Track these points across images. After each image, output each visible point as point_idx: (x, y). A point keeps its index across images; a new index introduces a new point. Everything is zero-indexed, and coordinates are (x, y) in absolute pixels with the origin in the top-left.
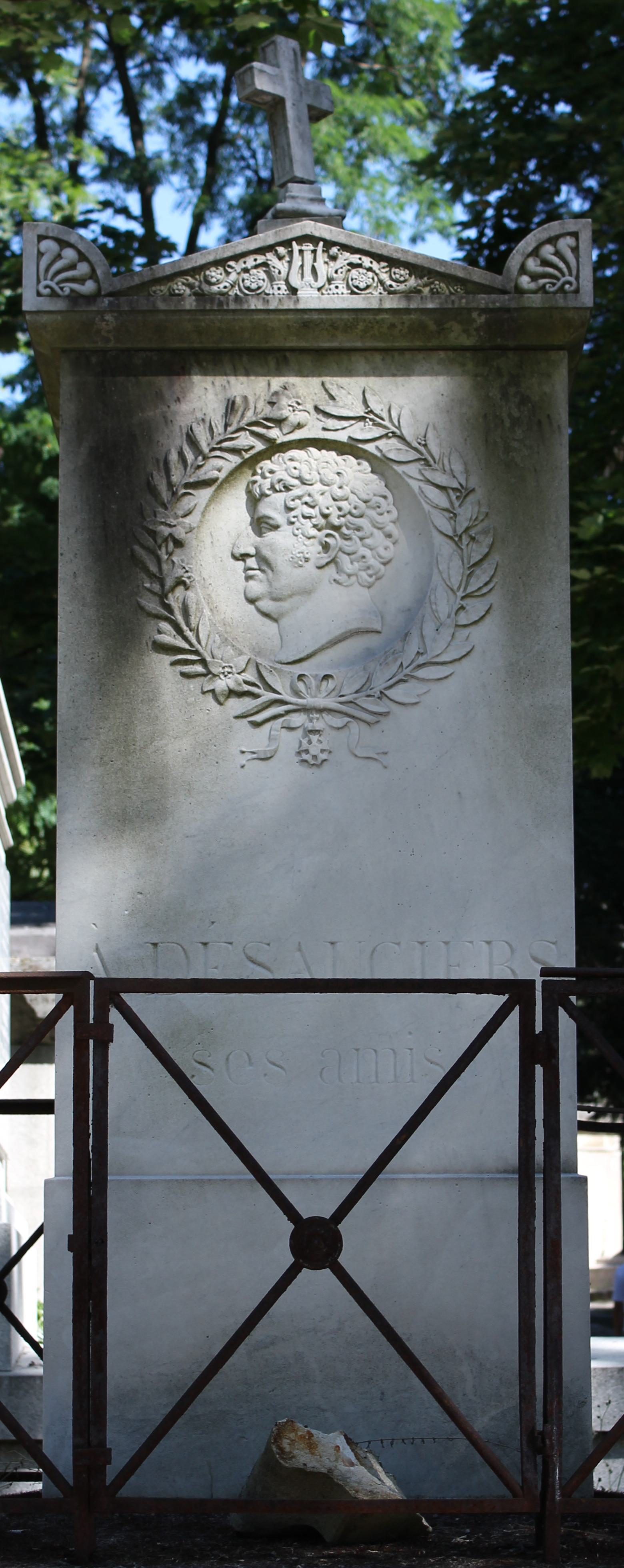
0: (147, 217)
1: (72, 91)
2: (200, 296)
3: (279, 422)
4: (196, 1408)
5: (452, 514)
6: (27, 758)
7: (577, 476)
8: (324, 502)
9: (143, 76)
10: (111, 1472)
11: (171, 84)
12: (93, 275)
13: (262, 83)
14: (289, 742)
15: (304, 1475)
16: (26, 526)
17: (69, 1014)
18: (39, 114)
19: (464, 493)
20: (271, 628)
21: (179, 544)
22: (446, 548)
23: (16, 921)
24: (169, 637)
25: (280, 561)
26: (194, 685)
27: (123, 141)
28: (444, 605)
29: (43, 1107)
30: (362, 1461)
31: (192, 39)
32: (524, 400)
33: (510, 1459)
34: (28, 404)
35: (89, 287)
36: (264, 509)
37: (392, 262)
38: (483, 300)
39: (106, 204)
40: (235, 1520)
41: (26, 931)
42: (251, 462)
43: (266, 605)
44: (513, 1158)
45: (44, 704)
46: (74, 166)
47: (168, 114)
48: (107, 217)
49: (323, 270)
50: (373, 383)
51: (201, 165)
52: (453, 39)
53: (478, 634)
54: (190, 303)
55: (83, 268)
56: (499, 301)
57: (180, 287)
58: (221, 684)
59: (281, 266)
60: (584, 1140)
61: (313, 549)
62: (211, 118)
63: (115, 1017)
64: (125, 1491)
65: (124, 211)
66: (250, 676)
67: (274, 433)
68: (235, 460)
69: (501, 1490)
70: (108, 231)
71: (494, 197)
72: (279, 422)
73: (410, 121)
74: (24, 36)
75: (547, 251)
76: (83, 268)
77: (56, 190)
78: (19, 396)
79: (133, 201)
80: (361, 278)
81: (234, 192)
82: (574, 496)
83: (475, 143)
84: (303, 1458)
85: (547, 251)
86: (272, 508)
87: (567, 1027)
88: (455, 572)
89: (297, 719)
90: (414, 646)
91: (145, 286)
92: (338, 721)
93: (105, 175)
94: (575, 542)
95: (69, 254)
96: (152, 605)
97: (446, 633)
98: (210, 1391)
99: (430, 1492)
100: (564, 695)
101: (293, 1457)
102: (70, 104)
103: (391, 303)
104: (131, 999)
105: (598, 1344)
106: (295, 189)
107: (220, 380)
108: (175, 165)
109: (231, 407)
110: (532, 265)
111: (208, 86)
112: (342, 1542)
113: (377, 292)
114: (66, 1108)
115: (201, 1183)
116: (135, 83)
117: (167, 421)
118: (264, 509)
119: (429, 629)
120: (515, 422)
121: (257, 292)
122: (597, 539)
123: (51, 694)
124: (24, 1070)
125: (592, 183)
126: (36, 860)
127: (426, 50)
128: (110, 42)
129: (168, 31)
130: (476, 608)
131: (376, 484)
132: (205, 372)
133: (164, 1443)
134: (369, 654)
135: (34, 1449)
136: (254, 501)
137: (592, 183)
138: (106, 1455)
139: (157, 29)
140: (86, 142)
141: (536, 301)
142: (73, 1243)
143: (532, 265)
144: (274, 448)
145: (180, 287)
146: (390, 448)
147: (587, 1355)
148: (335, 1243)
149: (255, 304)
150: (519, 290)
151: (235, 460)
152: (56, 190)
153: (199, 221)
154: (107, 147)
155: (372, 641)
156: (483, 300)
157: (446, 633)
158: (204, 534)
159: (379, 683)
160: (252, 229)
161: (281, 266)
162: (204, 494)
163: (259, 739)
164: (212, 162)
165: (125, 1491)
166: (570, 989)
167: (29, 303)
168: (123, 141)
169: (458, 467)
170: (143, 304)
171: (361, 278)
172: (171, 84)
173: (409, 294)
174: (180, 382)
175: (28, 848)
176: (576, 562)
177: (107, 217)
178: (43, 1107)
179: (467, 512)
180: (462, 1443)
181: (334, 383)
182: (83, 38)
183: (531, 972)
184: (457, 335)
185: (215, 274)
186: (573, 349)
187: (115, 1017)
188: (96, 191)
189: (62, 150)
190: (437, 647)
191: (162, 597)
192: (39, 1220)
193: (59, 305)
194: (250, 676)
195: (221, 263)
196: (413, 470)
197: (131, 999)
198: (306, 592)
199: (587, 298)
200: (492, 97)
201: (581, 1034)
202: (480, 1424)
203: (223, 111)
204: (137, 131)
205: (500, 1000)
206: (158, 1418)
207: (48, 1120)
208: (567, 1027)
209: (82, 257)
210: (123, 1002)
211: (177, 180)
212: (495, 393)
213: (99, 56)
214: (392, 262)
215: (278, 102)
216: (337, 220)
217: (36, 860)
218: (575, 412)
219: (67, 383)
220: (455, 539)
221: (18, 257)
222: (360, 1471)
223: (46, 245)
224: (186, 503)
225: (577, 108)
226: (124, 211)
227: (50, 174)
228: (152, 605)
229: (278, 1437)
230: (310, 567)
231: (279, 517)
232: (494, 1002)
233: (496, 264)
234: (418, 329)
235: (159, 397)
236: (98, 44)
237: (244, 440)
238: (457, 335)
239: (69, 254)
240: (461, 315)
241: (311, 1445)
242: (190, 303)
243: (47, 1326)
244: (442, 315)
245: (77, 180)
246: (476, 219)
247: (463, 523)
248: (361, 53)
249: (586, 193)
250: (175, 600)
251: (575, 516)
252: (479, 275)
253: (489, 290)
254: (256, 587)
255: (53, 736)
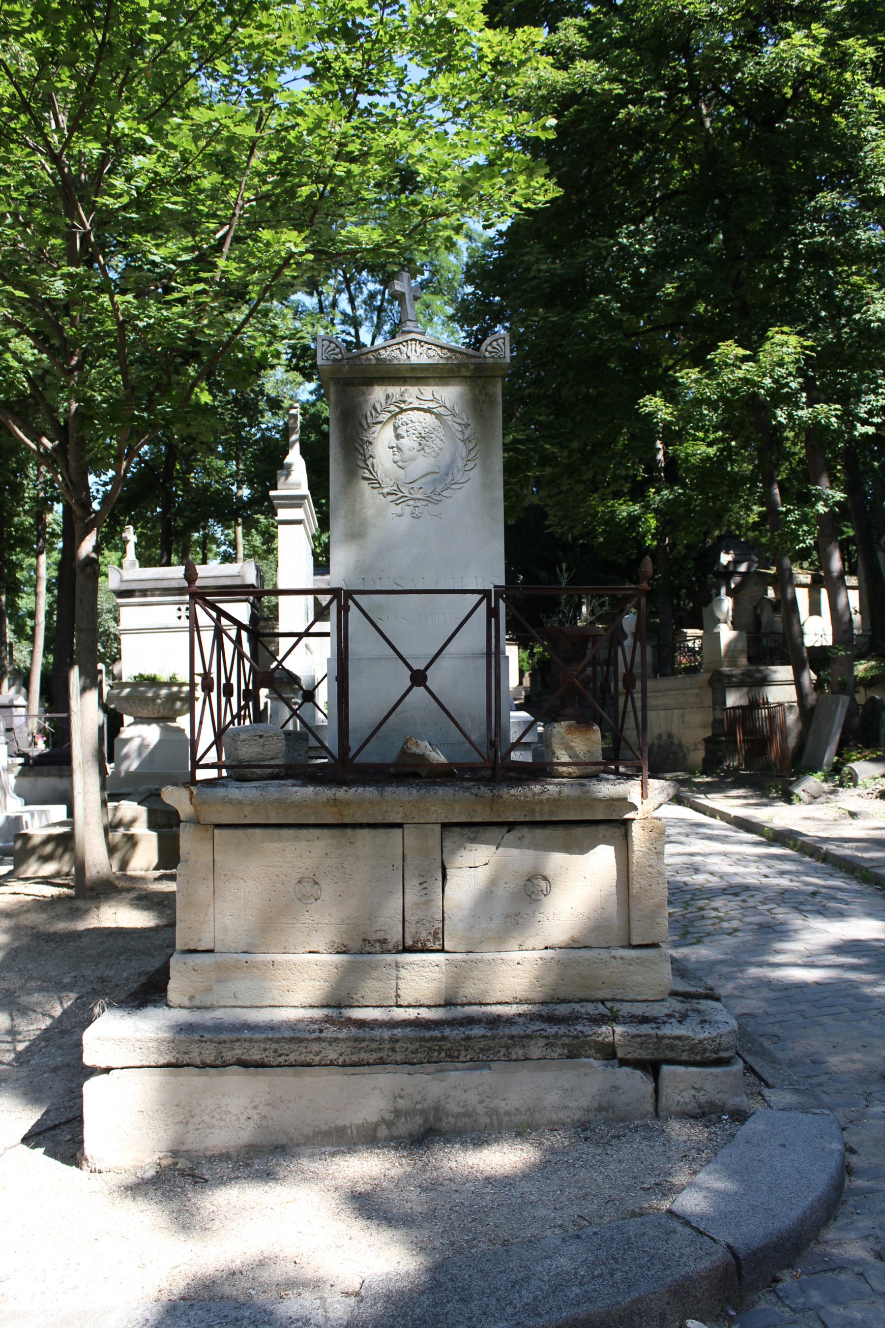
0: (357, 336)
1: (332, 294)
2: (377, 359)
3: (404, 402)
4: (379, 734)
5: (463, 433)
6: (318, 519)
7: (505, 422)
8: (420, 429)
9: (355, 289)
10: (351, 754)
11: (365, 291)
12: (341, 352)
13: (397, 288)
14: (408, 510)
15: (415, 755)
16: (317, 441)
17: (335, 602)
18: (320, 302)
19: (467, 426)
20: (402, 471)
21: (370, 443)
22: (461, 444)
23: (315, 574)
24: (367, 475)
25: (405, 449)
26: (376, 491)
27: (349, 311)
28: (460, 463)
29: (326, 635)
30: (434, 750)
31: (373, 276)
32: (487, 394)
33: (484, 749)
34: (317, 400)
35: (339, 356)
36: (399, 431)
37: (442, 348)
38: (473, 360)
39: (343, 332)
40: (392, 770)
41: (318, 577)
42: (395, 416)
43: (400, 464)
44: (484, 650)
45: (323, 501)
46: (332, 320)
47: (365, 302)
48: (344, 336)
49: (419, 350)
50: (436, 388)
51: (375, 319)
52: (461, 277)
53: (471, 473)
54: (374, 362)
55: (337, 350)
56: (479, 361)
57: (370, 356)
58: (385, 491)
59: (404, 349)
60: (508, 648)
61: (416, 445)
62: (379, 303)
63: (350, 603)
64: (355, 761)
65: (349, 334)
66: (395, 488)
67: (402, 406)
68: (389, 415)
69: (482, 760)
70: (344, 341)
71: (475, 328)
72: (404, 402)
73: (446, 303)
74: (316, 273)
75: (495, 344)
76: (337, 350)
77: (326, 328)
78: (314, 397)
79: (353, 332)
80: (431, 353)
81: (387, 328)
82: (504, 429)
83: (468, 310)
84: (415, 750)
85: (495, 344)
86: (402, 431)
87: (502, 605)
88: (463, 452)
89: (411, 502)
90: (450, 478)
91: (358, 356)
92: (425, 503)
93: (343, 323)
94: (504, 445)
95: (333, 345)
96: (362, 464)
97: (461, 473)
98: (383, 728)
99: (457, 760)
100: (500, 494)
101: (178, 1123)
102: (331, 298)
103: (442, 361)
104: (356, 597)
105: (512, 714)
106: (409, 323)
107: (384, 388)
108: (366, 319)
109: (388, 397)
110: (489, 348)
111: (379, 292)
112: (428, 777)
113: (437, 358)
114: (334, 635)
115: (379, 659)
116: (353, 292)
117: (366, 402)
118: (399, 431)
119: (455, 471)
120: (484, 402)
121: (396, 358)
122: (511, 443)
123: (327, 498)
124: (317, 624)
125: (507, 324)
126: (320, 555)
127: (450, 281)
128: (345, 277)
129: (364, 273)
130: (471, 465)
131: (437, 422)
132: (379, 385)
133: (368, 746)
134: (435, 480)
135: (323, 747)
136: (396, 428)
137: (507, 324)
138: (348, 749)
139: (360, 273)
140: (337, 311)
141: (491, 361)
142: (337, 679)
143: (489, 348)
144: (402, 411)
145: (370, 356)
146: (442, 410)
147: (509, 717)
148: (425, 678)
149: (396, 362)
150: (485, 357)
151: (389, 415)
152: (326, 328)
153: (374, 338)
154: (344, 313)
155: (436, 476)
156: (473, 360)
157: (461, 473)
158: (379, 440)
159: (438, 490)
160: (393, 337)
161: (404, 349)
162: (380, 426)
163: (398, 510)
164: (379, 317)
165: (355, 761)
166: (502, 592)
167: (319, 361)
168: (349, 311)
169: (465, 417)
170: (358, 362)
171: (431, 353)
172: (365, 291)
173: (448, 358)
174: (370, 388)
175: (318, 550)
176: (504, 451)
177: (344, 336)
178: (326, 635)
179: (468, 432)
180: (467, 744)
181: (422, 388)
182: (335, 277)
183: (491, 587)
184: (464, 372)
185: (382, 352)
186: (503, 379)
187: (350, 603)
188: (339, 328)
189: (328, 314)
190: (459, 477)
191: (365, 461)
192: (325, 672)
193: (329, 363)
194: (395, 488)
195: (384, 348)
196: (449, 418)
197: (356, 597)
198: (413, 459)
199: (508, 360)
200: (473, 293)
201: (507, 607)
202: (473, 738)
203: (382, 301)
204: (354, 308)
205: (480, 596)
206: (366, 737)
207: (328, 639)
208: (502, 605)
209: (337, 346)
210: (176, 838)
211: (367, 323)
212: (477, 392)
213: (340, 282)
214: (442, 348)
215: (403, 294)
216: (423, 334)
217: (320, 555)
218: (503, 401)
219: (332, 389)
220: (464, 441)
221: (315, 350)
222: (433, 753)
223: (325, 342)
224: (373, 429)
225: (503, 298)
226: (349, 334)
227: (324, 322)
228: (362, 464)
229: (406, 743)
230: (415, 451)
231: (404, 434)
232: (477, 597)
233: (478, 349)
234: (451, 370)
235: (364, 394)
236: (340, 278)
237: (392, 408)
238: (464, 372)
239: (333, 345)
240: (465, 365)
241: (417, 745)
242: (374, 362)
243: (328, 709)
244: (459, 366)
245: (333, 325)
246: (469, 336)
247: (466, 436)
248: (429, 281)
249: (505, 328)
250: (369, 462)
251: (504, 435)
252: (470, 351)
253: (475, 357)
254: (397, 458)
255: (328, 513)
